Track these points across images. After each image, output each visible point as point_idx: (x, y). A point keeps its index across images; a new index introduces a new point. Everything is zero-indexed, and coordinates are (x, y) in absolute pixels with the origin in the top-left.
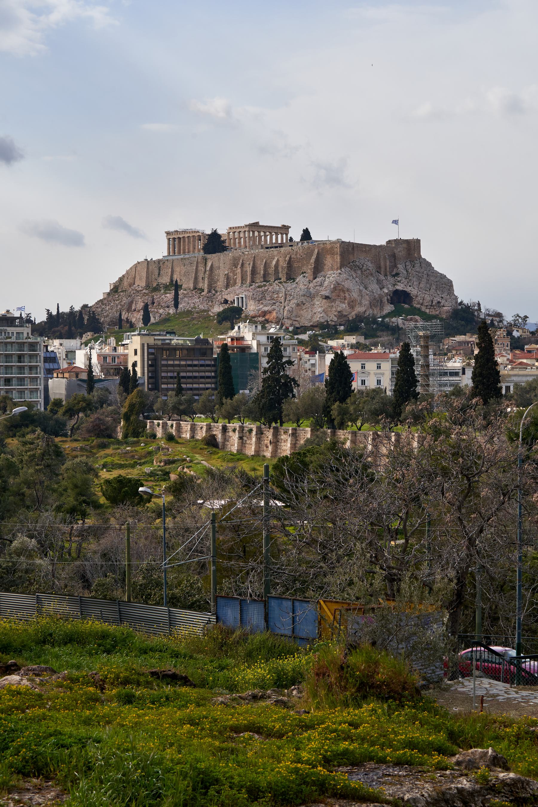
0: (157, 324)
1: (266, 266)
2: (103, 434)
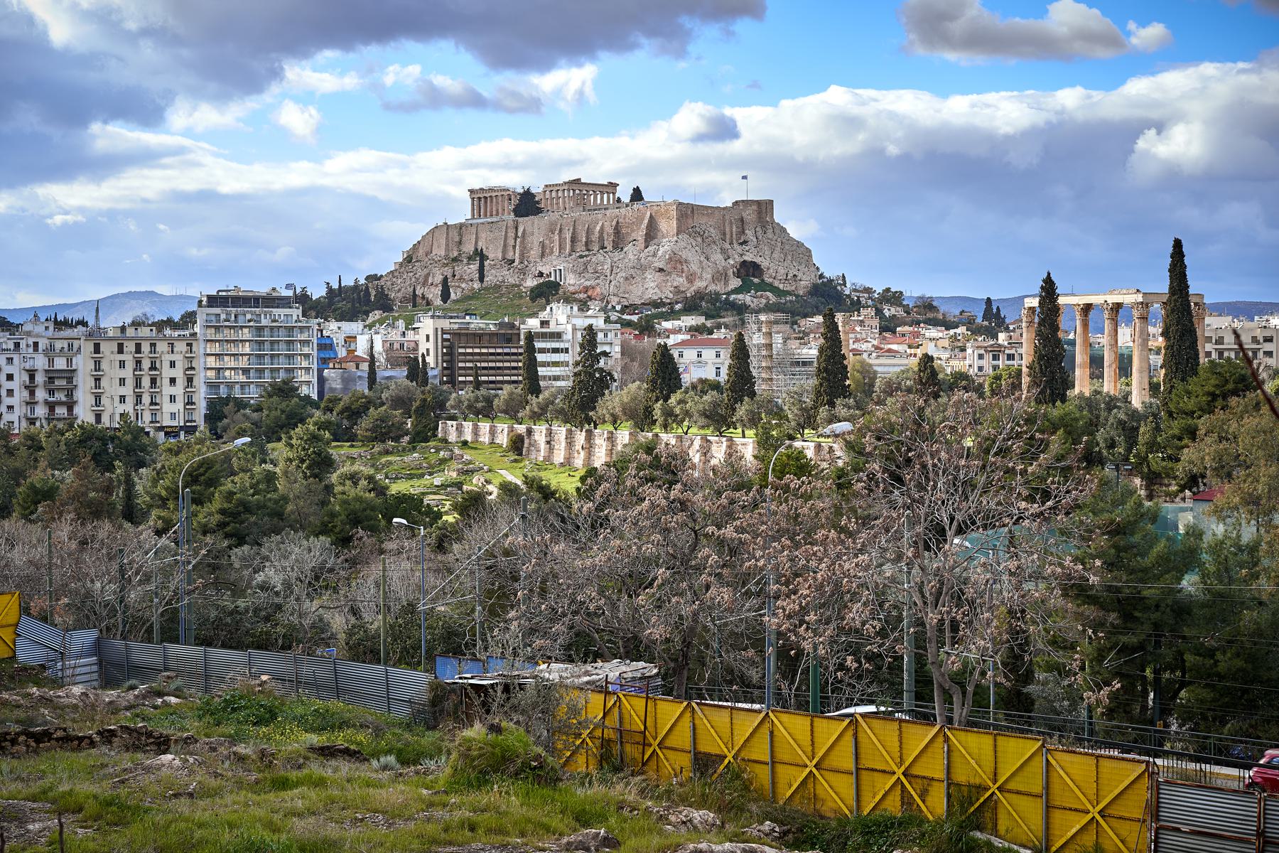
0: (456, 302)
1: (589, 232)
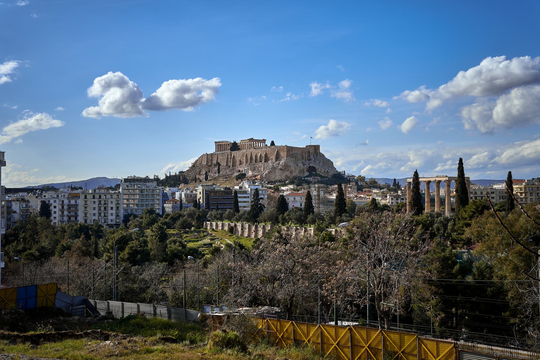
1: (256, 156)
2: (186, 226)
